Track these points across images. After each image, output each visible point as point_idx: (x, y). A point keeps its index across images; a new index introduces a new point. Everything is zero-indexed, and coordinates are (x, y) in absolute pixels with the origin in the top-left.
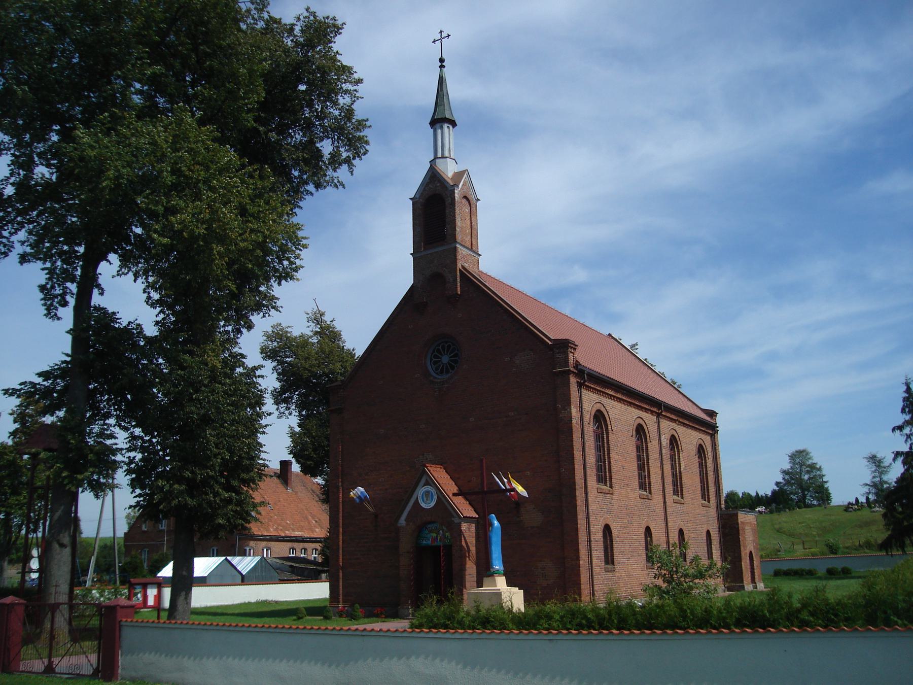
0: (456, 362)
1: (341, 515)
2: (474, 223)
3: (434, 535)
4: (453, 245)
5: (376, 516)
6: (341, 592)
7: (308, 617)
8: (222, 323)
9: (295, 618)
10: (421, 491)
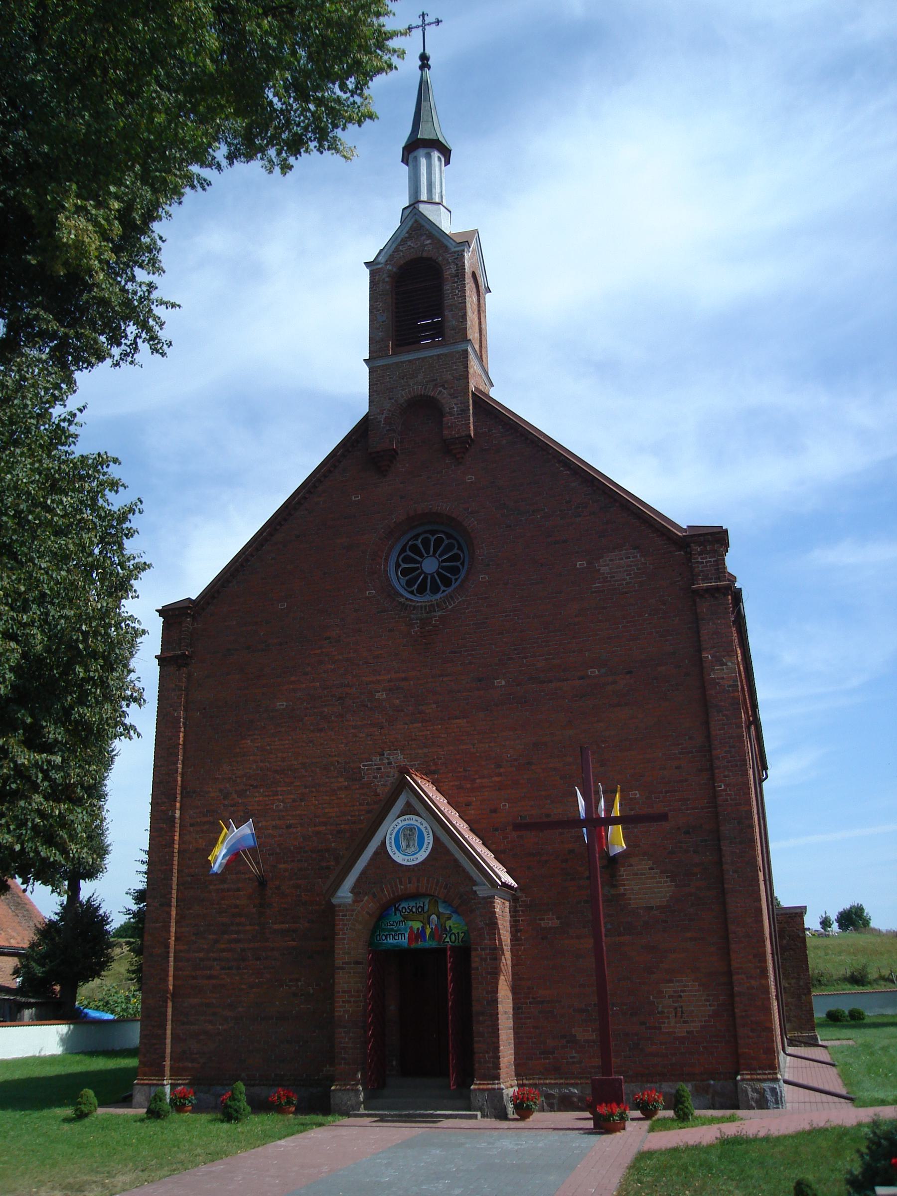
0: (455, 571)
1: (175, 879)
2: (483, 326)
3: (417, 925)
4: (460, 347)
5: (262, 883)
6: (168, 1051)
7: (101, 1111)
8: (92, 202)
9: (69, 1112)
10: (392, 827)
